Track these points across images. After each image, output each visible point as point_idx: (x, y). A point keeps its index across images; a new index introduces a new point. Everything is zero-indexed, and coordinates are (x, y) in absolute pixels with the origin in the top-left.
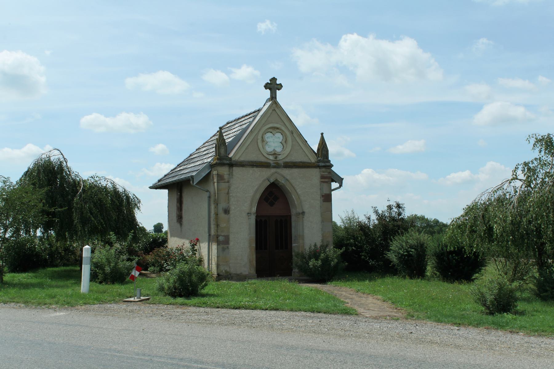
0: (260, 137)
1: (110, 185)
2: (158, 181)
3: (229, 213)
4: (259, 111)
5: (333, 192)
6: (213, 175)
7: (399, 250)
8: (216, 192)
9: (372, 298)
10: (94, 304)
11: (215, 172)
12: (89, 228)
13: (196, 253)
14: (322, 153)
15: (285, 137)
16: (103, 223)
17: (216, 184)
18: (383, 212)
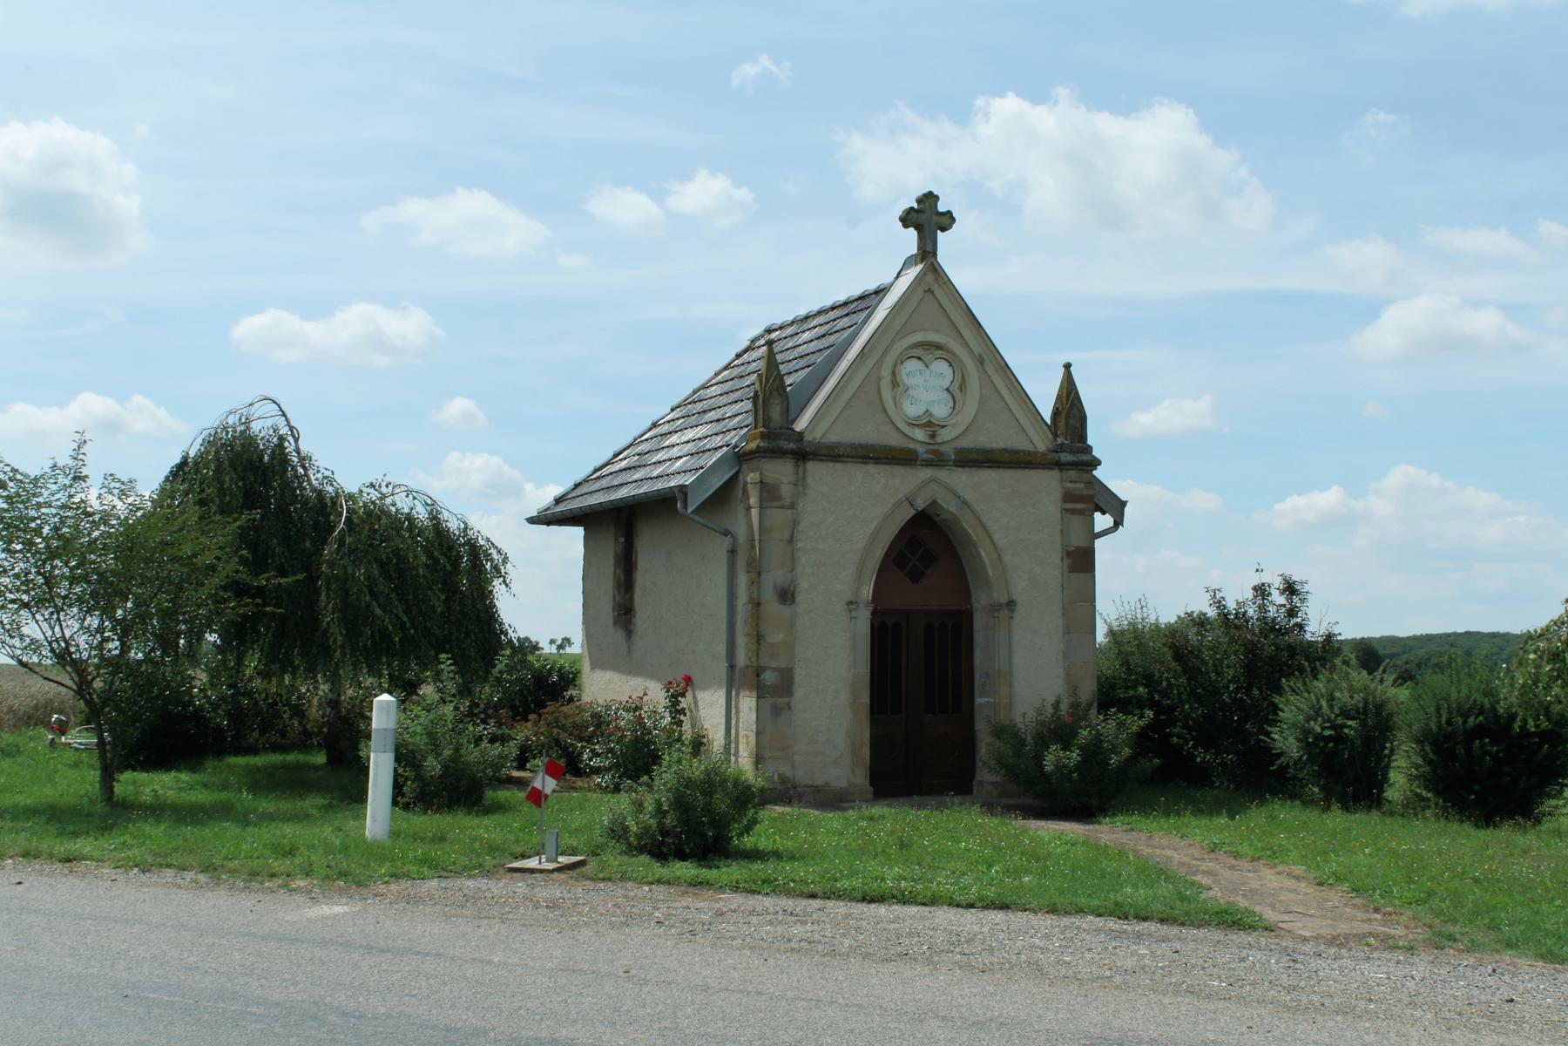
0: (886, 372)
1: (421, 513)
2: (555, 500)
3: (794, 602)
4: (881, 292)
5: (1098, 543)
6: (746, 484)
7: (1308, 722)
8: (757, 537)
9: (1273, 871)
10: (423, 879)
11: (751, 475)
12: (368, 640)
13: (682, 721)
14: (1067, 423)
15: (960, 375)
16: (408, 625)
17: (754, 513)
18: (1238, 603)
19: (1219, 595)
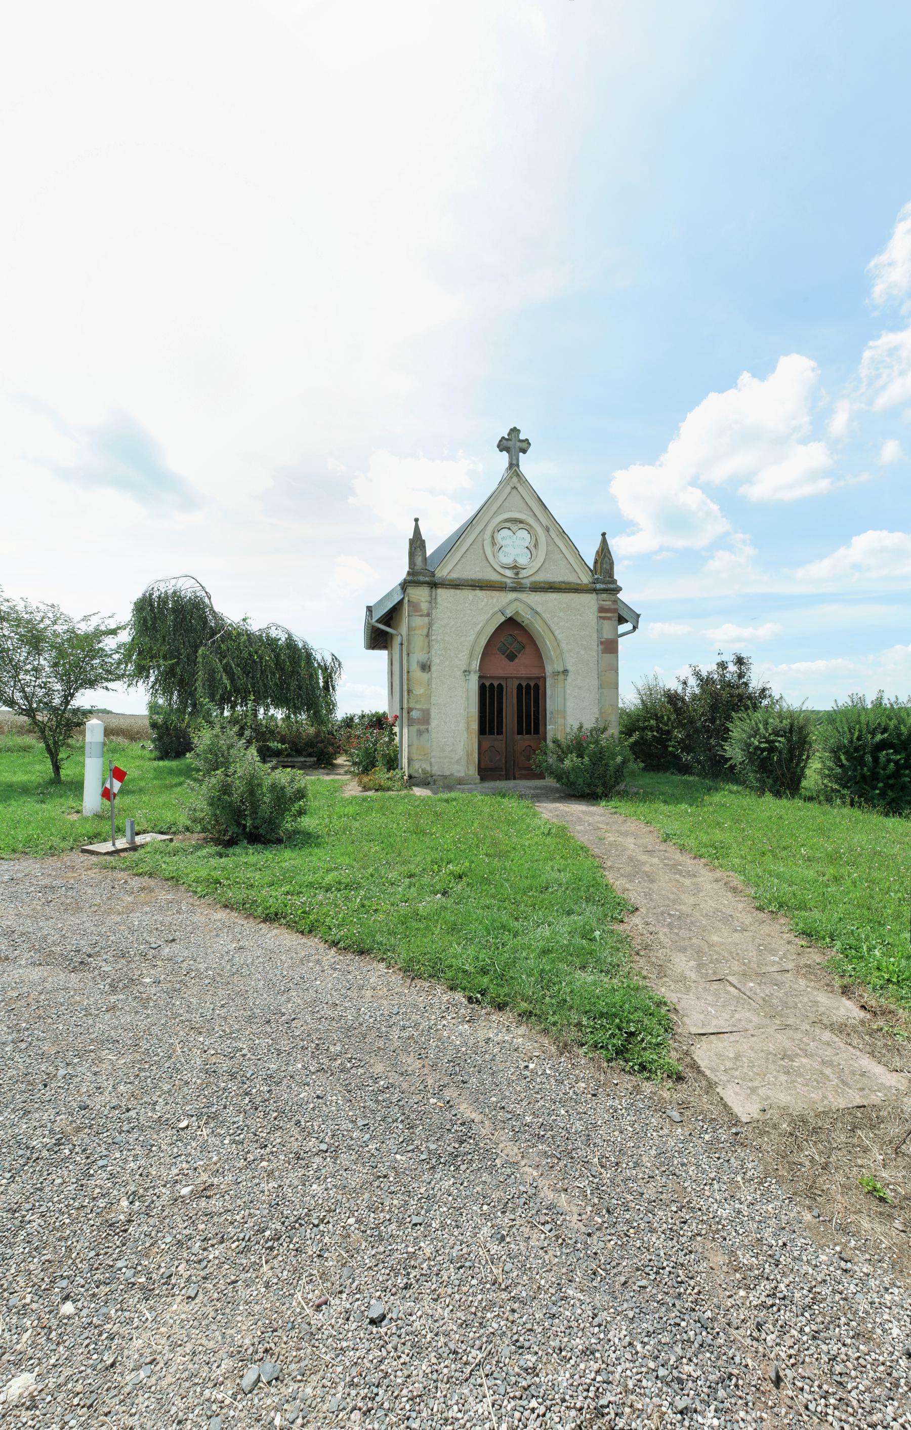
7: (750, 738)
19: (697, 669)
